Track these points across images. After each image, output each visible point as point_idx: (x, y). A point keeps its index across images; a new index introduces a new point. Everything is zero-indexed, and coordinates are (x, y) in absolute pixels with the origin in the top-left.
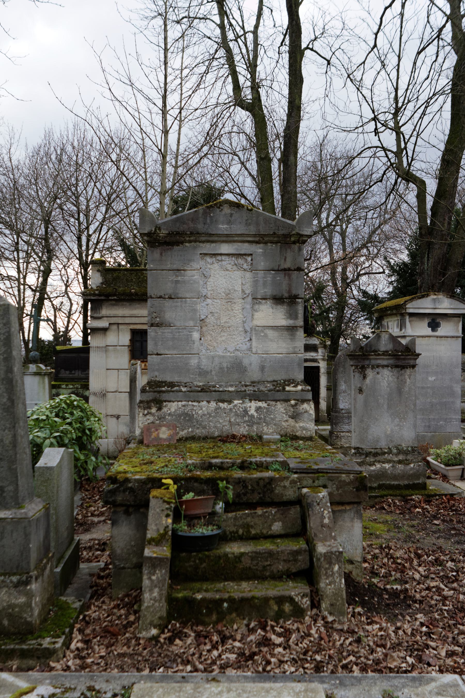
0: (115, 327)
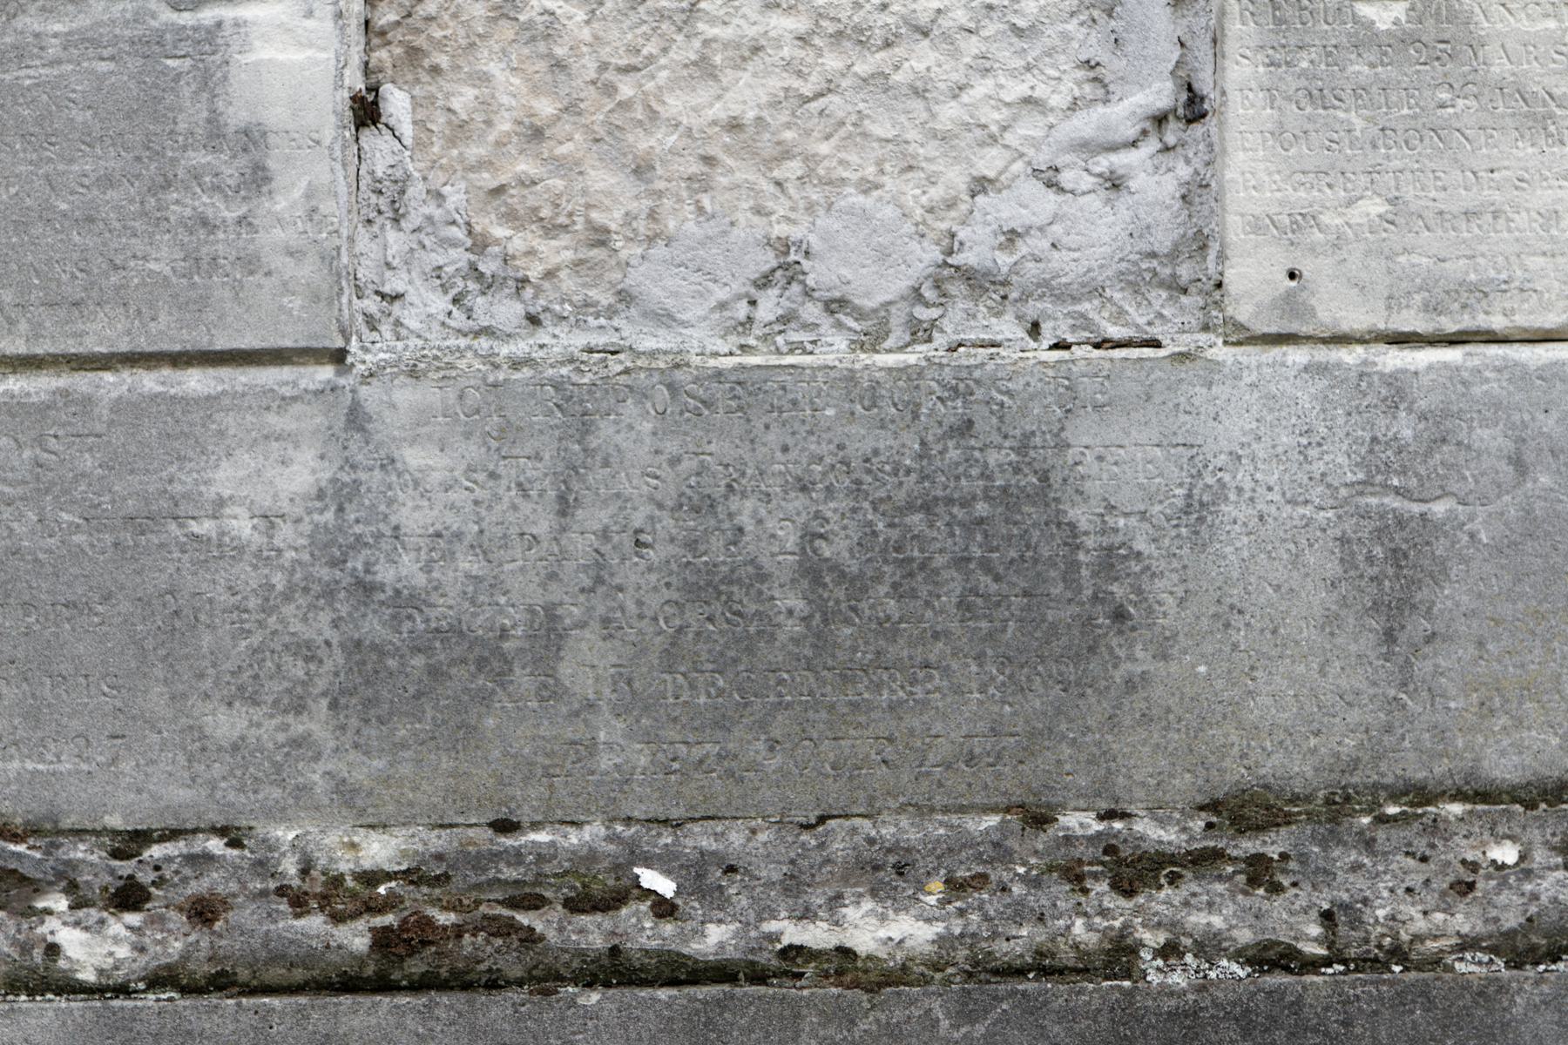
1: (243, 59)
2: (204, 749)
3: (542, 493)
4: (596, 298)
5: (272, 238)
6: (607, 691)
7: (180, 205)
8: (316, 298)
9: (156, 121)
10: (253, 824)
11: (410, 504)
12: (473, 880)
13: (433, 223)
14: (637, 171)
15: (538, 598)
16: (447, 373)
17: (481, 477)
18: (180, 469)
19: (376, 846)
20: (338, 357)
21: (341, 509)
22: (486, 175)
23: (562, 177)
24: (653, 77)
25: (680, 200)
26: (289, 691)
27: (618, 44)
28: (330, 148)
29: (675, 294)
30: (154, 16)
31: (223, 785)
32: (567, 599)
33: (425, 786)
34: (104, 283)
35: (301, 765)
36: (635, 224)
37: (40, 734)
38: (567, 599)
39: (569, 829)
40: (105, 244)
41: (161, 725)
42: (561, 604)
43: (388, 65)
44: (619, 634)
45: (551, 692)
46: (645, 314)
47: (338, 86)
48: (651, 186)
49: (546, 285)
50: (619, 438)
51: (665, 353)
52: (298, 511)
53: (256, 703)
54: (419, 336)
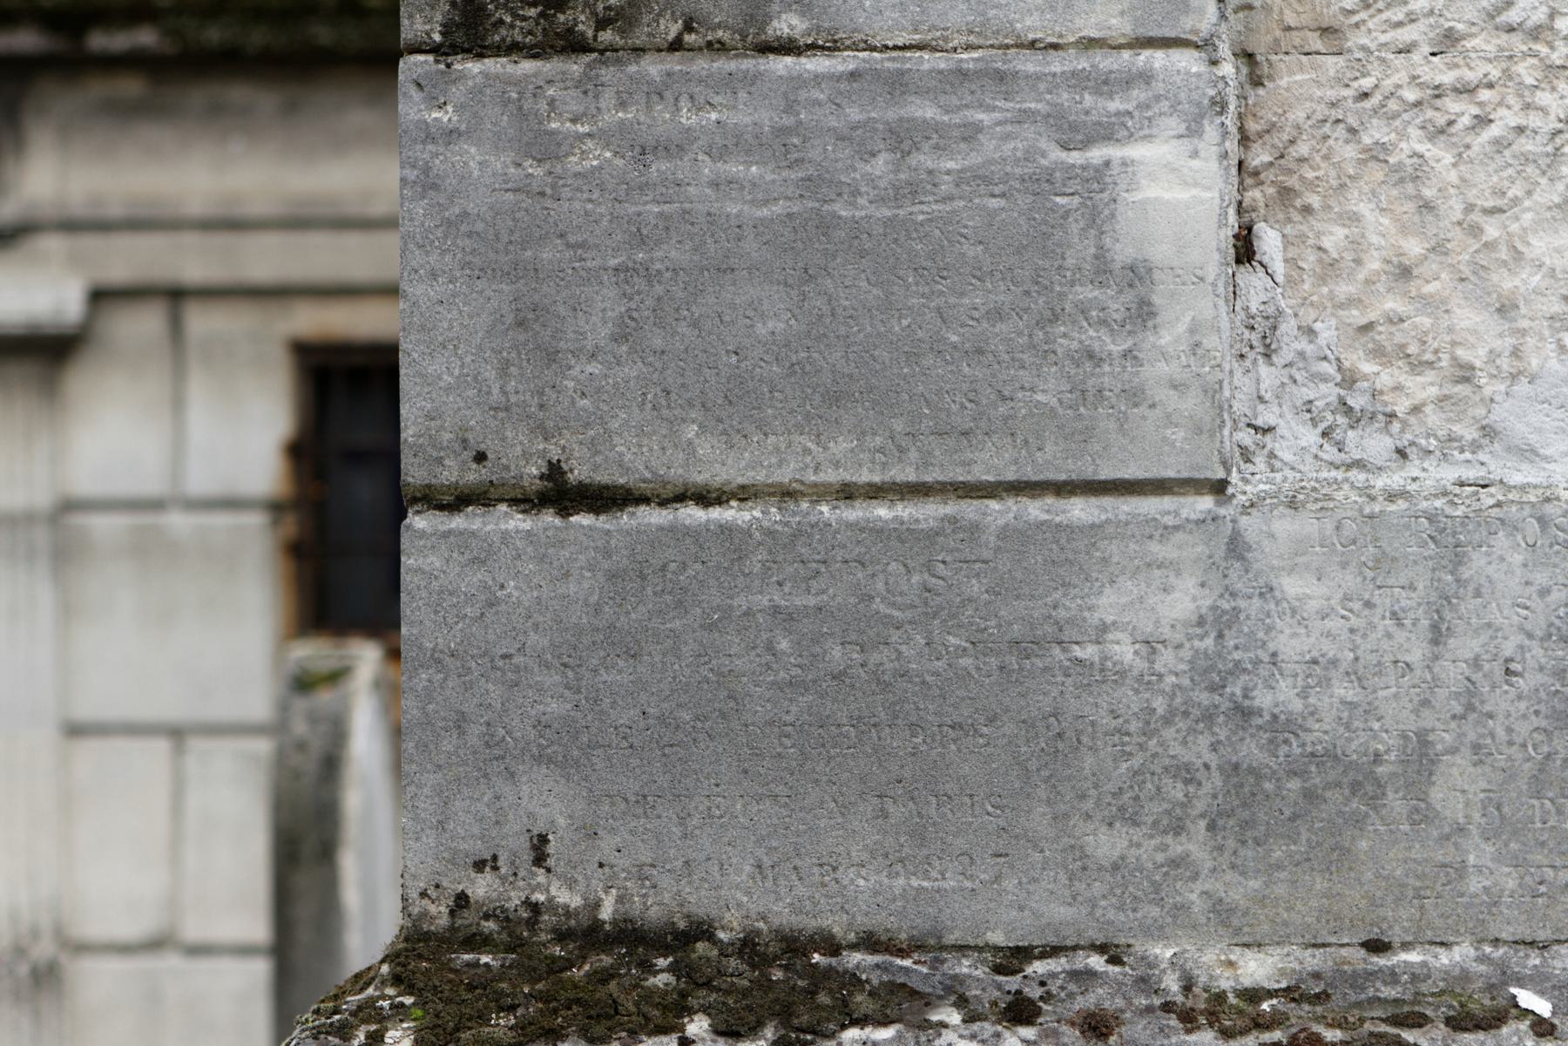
0: (140, 326)
1: (1130, 197)
2: (1084, 868)
3: (1416, 622)
4: (1460, 433)
5: (1155, 372)
6: (1477, 816)
7: (1067, 339)
8: (1199, 431)
9: (1045, 256)
10: (1131, 941)
11: (1287, 631)
12: (1353, 997)
13: (1305, 359)
14: (1501, 310)
15: (1411, 724)
16: (1325, 504)
17: (1357, 606)
18: (1065, 595)
19: (1252, 965)
20: (1219, 488)
21: (1220, 636)
22: (1355, 312)
23: (1429, 315)
24: (1517, 219)
25: (1542, 339)
26: (1168, 812)
27: (1484, 186)
28: (1214, 285)
29: (1539, 430)
30: (1044, 155)
31: (1103, 903)
32: (1438, 725)
33: (1299, 906)
34: (993, 412)
35: (1179, 885)
36: (1498, 362)
37: (925, 852)
38: (1438, 725)
39: (1439, 950)
40: (993, 375)
41: (1043, 844)
42: (1433, 730)
43: (1261, 204)
44: (1489, 760)
45: (1422, 815)
46: (1509, 449)
47: (1222, 223)
48: (1514, 325)
49: (1412, 420)
50: (1490, 570)
51: (1535, 487)
52: (1179, 637)
53: (1136, 824)
54: (1293, 468)
